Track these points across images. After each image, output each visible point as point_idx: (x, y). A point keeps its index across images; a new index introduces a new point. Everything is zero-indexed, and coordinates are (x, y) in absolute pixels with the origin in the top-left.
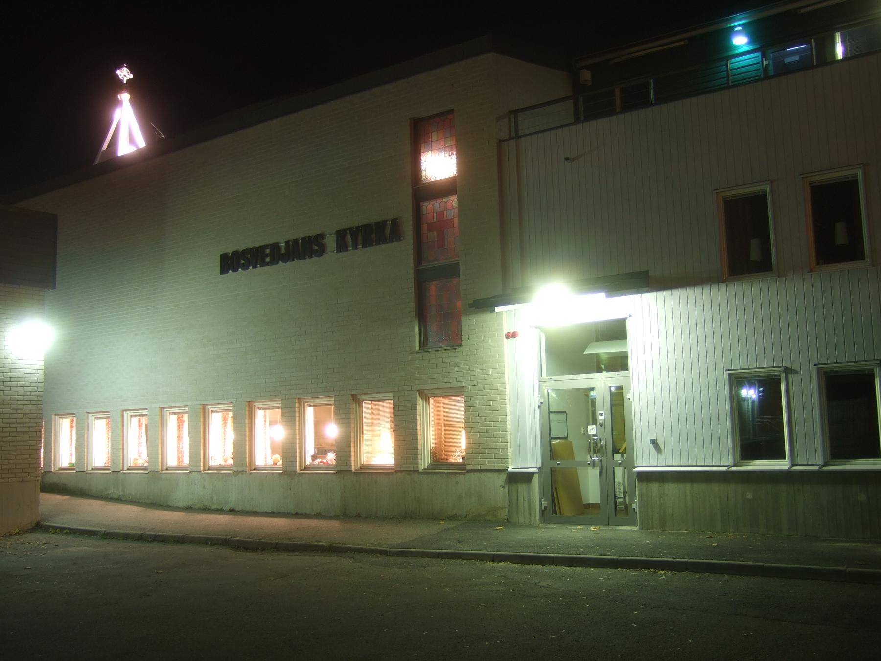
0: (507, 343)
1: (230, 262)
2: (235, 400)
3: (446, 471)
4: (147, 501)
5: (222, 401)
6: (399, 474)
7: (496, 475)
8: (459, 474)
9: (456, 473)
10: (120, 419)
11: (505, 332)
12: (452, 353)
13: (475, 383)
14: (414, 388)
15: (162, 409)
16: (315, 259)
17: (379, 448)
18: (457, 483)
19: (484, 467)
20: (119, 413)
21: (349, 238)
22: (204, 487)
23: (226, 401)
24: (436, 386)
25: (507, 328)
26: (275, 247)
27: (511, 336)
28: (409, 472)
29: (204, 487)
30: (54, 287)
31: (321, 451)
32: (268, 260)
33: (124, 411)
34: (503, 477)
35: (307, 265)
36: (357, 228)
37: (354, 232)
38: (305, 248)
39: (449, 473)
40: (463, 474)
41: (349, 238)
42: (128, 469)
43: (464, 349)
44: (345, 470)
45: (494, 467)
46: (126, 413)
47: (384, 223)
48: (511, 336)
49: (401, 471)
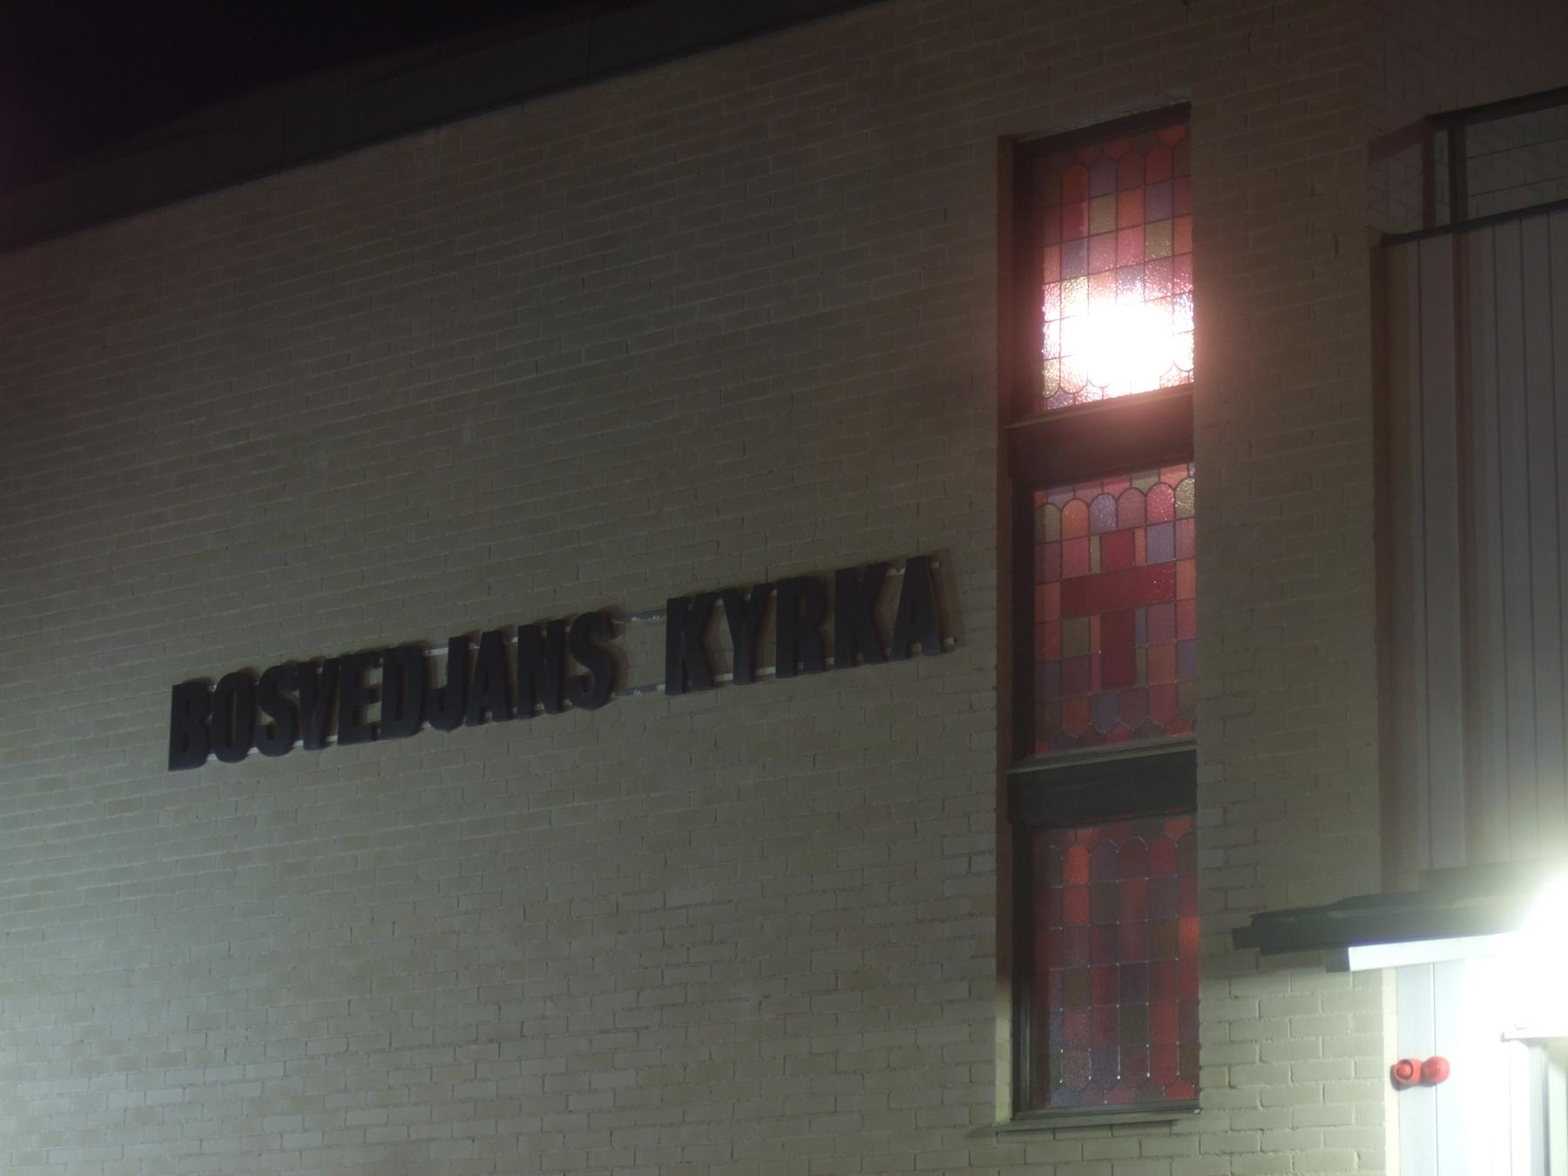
1: (213, 721)
11: (1391, 1058)
16: (576, 716)
26: (406, 662)
27: (1420, 1074)
35: (544, 741)
36: (762, 590)
37: (747, 606)
38: (536, 669)
41: (722, 632)
47: (877, 573)
48: (1420, 1074)
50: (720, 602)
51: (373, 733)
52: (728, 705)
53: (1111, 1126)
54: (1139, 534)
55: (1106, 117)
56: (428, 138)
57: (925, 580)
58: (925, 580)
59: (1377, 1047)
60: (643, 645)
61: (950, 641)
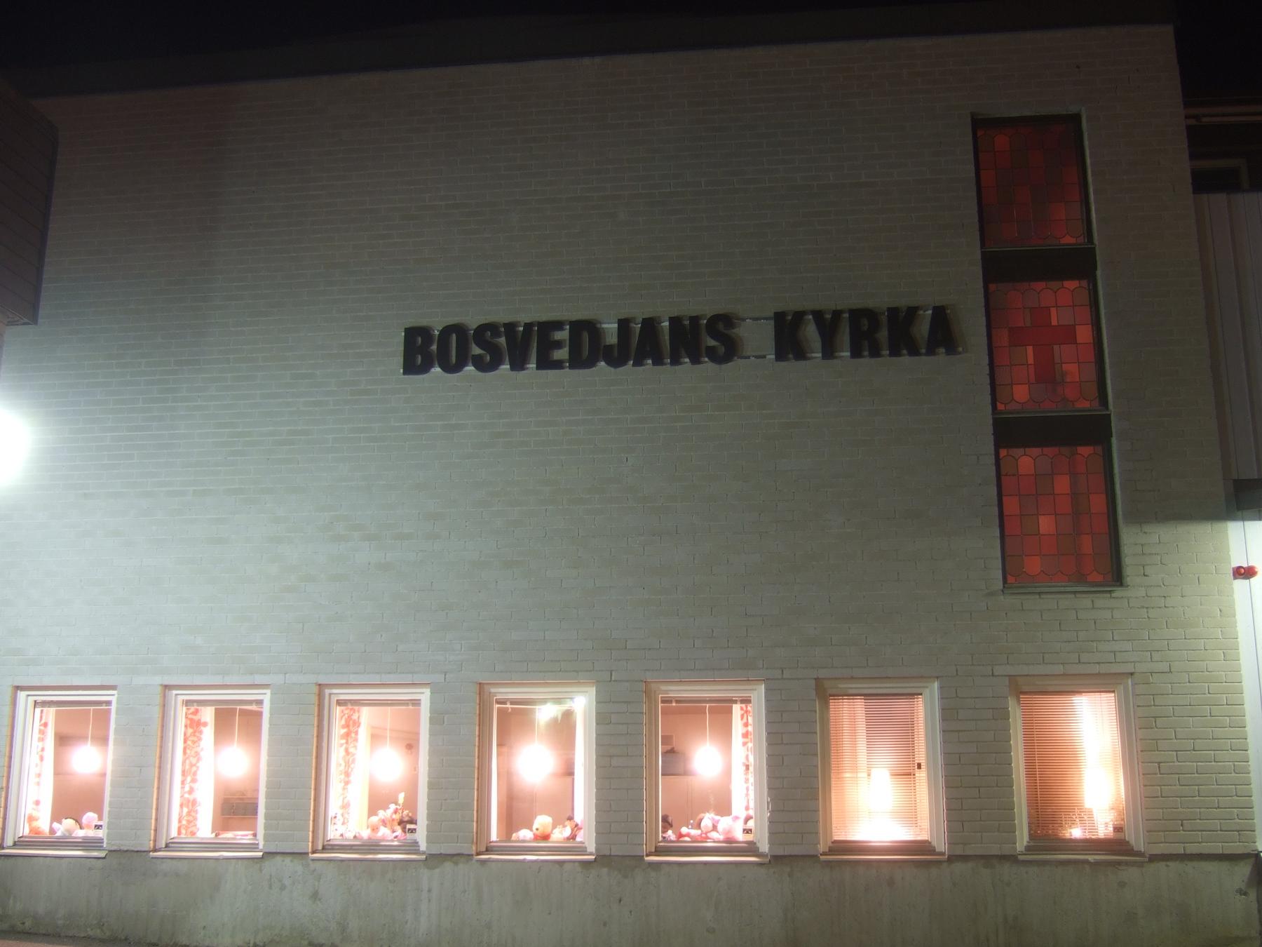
0: (1240, 584)
1: (424, 351)
2: (439, 678)
3: (1091, 858)
4: (98, 933)
5: (408, 679)
6: (959, 867)
7: (1225, 866)
8: (1127, 863)
9: (1119, 863)
10: (156, 712)
11: (1235, 564)
12: (1102, 601)
13: (1164, 667)
14: (999, 670)
15: (167, 687)
16: (708, 366)
17: (882, 801)
18: (1122, 884)
19: (1193, 849)
20: (9, 691)
21: (811, 332)
22: (315, 896)
23: (408, 679)
24: (1059, 669)
25: (1238, 560)
26: (585, 330)
27: (1246, 573)
28: (987, 859)
29: (315, 896)
30: (34, 320)
31: (71, 801)
32: (562, 354)
33: (18, 688)
34: (1244, 871)
35: (686, 377)
36: (837, 314)
37: (828, 324)
38: (698, 339)
39: (1097, 863)
40: (1134, 864)
41: (811, 332)
42: (16, 845)
43: (1135, 590)
44: (298, 846)
45: (1217, 848)
46: (22, 695)
47: (912, 312)
48: (1246, 573)
49: (964, 858)
50: (846, 315)
51: (558, 365)
52: (813, 370)
53: (1075, 593)
54: (1053, 311)
55: (1027, 113)
56: (586, 61)
57: (942, 318)
58: (942, 318)
59: (1227, 560)
60: (757, 336)
61: (960, 349)
